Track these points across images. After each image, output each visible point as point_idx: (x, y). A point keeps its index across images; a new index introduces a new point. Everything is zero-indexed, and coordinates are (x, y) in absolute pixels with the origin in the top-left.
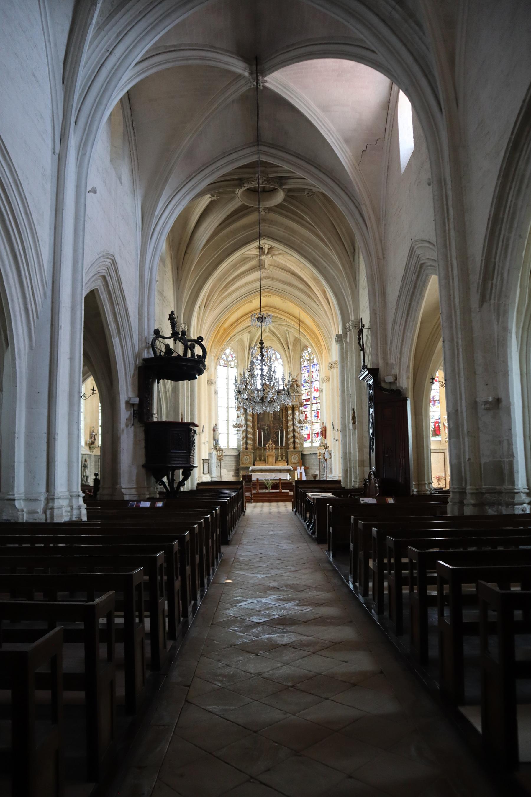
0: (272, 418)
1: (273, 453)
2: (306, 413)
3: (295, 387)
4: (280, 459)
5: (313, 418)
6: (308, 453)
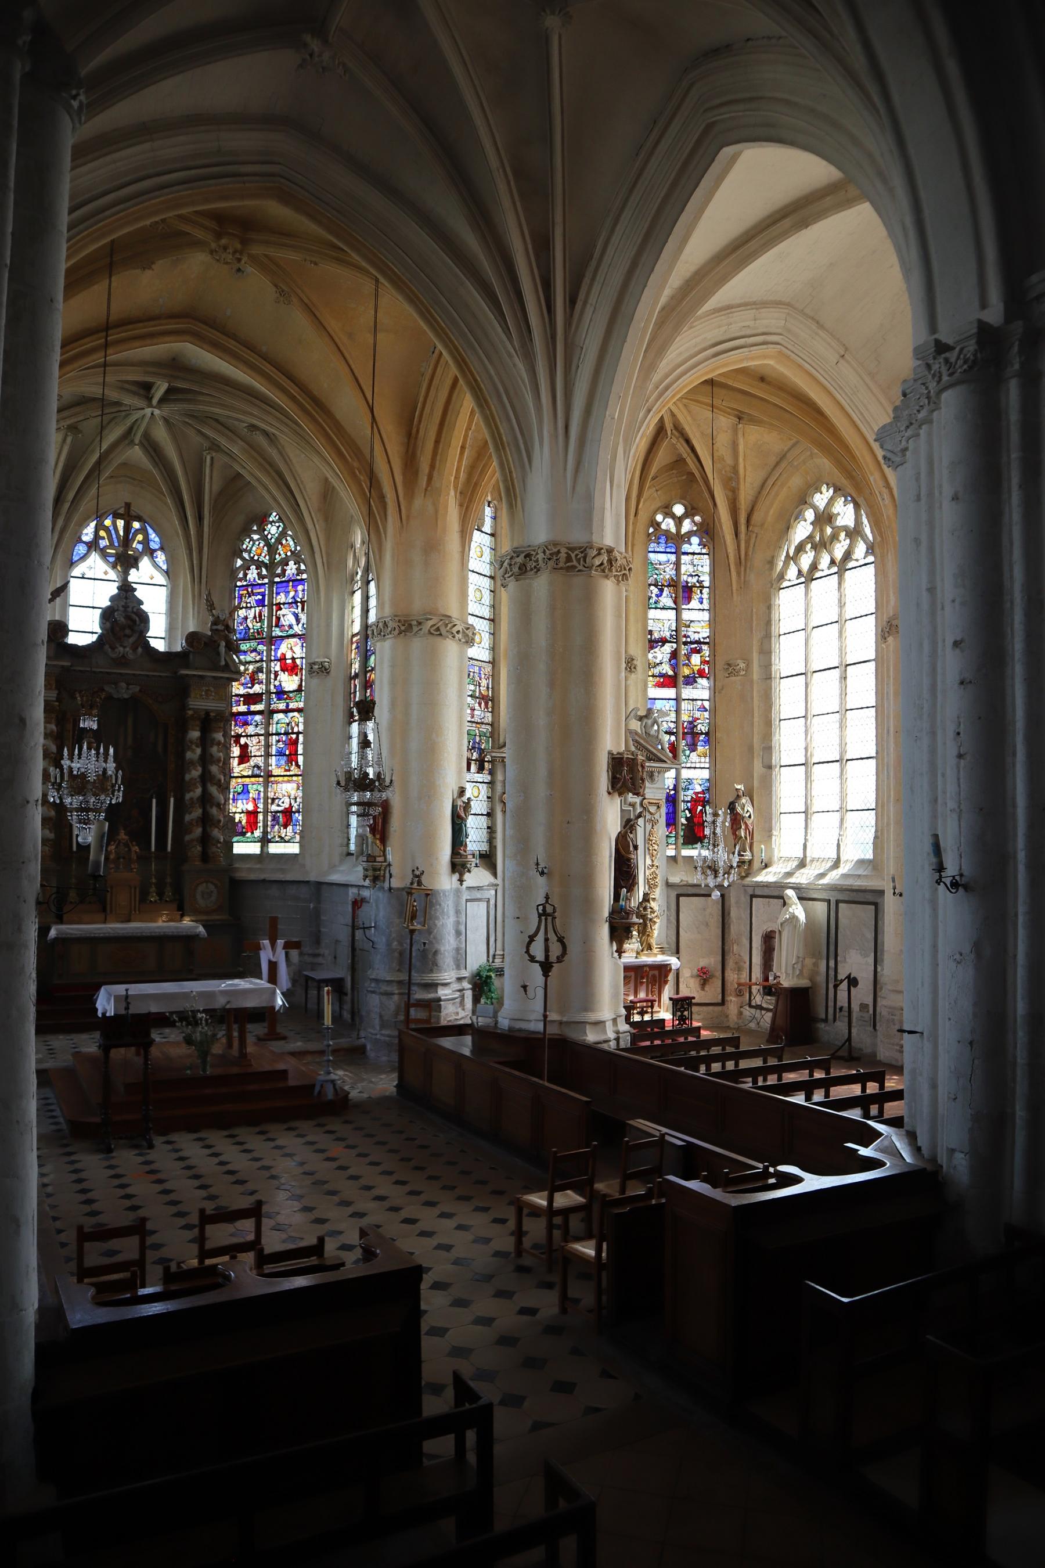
2: (243, 741)
6: (253, 876)
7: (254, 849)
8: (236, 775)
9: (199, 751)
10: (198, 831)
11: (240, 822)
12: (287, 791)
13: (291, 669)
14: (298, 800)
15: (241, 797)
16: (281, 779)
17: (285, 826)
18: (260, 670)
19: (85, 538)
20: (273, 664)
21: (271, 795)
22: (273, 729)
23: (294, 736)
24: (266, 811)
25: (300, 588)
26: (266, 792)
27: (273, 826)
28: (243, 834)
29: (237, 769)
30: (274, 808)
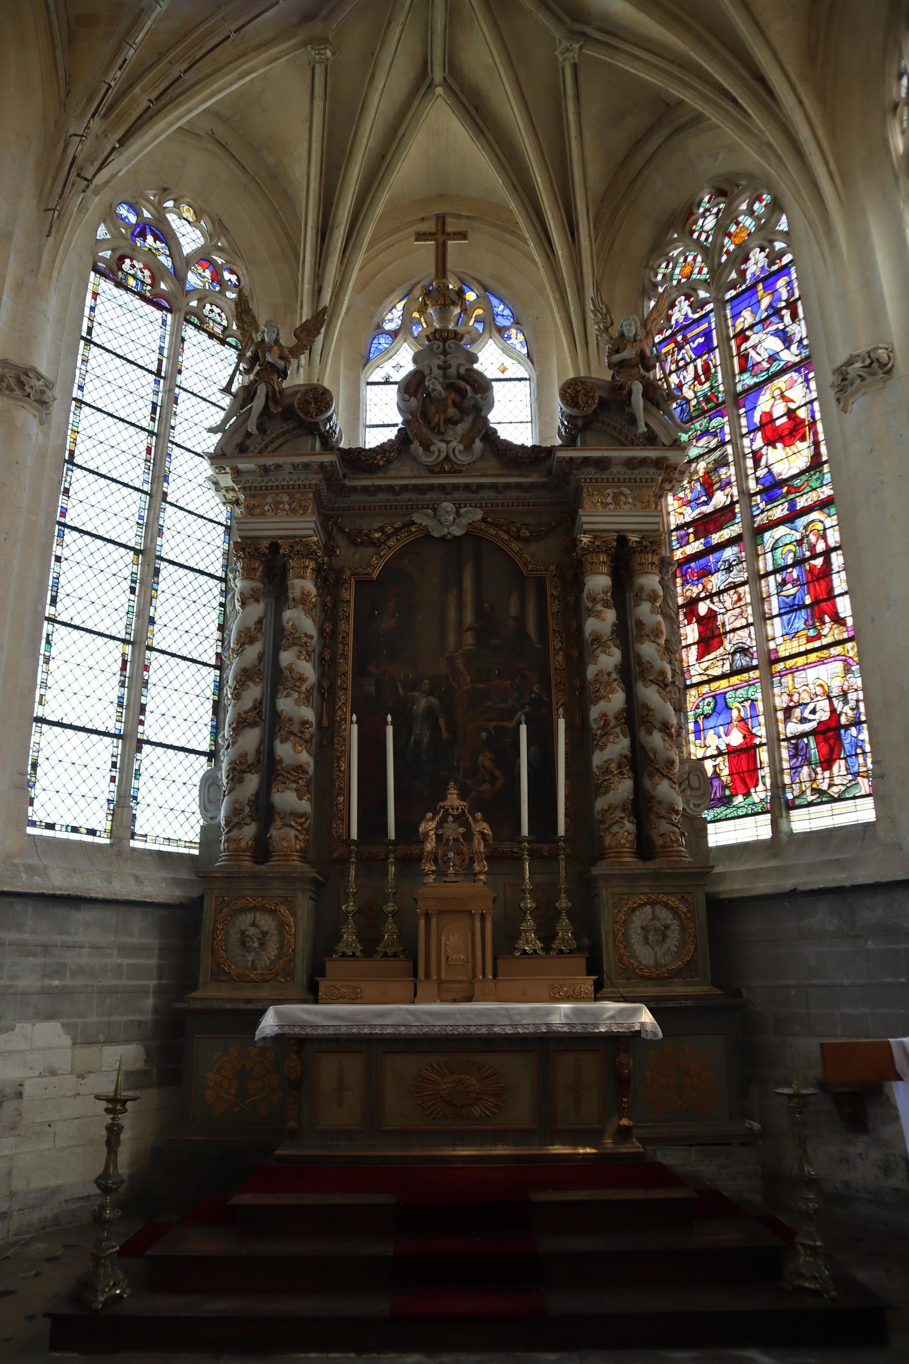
0: (469, 639)
1: (480, 889)
2: (702, 609)
3: (638, 401)
4: (530, 942)
5: (776, 628)
6: (762, 887)
7: (758, 829)
8: (695, 680)
9: (610, 615)
10: (624, 788)
11: (716, 775)
12: (823, 681)
13: (792, 430)
14: (852, 696)
15: (711, 722)
16: (800, 661)
17: (827, 764)
18: (723, 462)
19: (388, 326)
20: (746, 442)
21: (781, 702)
22: (766, 563)
23: (819, 562)
24: (774, 741)
25: (781, 282)
26: (768, 697)
27: (795, 769)
28: (726, 801)
29: (695, 666)
30: (793, 728)
